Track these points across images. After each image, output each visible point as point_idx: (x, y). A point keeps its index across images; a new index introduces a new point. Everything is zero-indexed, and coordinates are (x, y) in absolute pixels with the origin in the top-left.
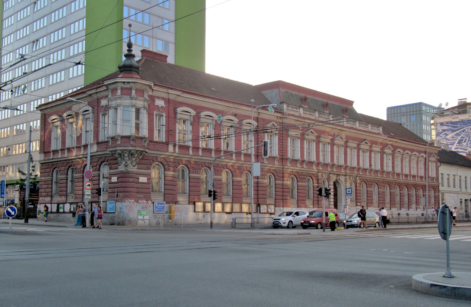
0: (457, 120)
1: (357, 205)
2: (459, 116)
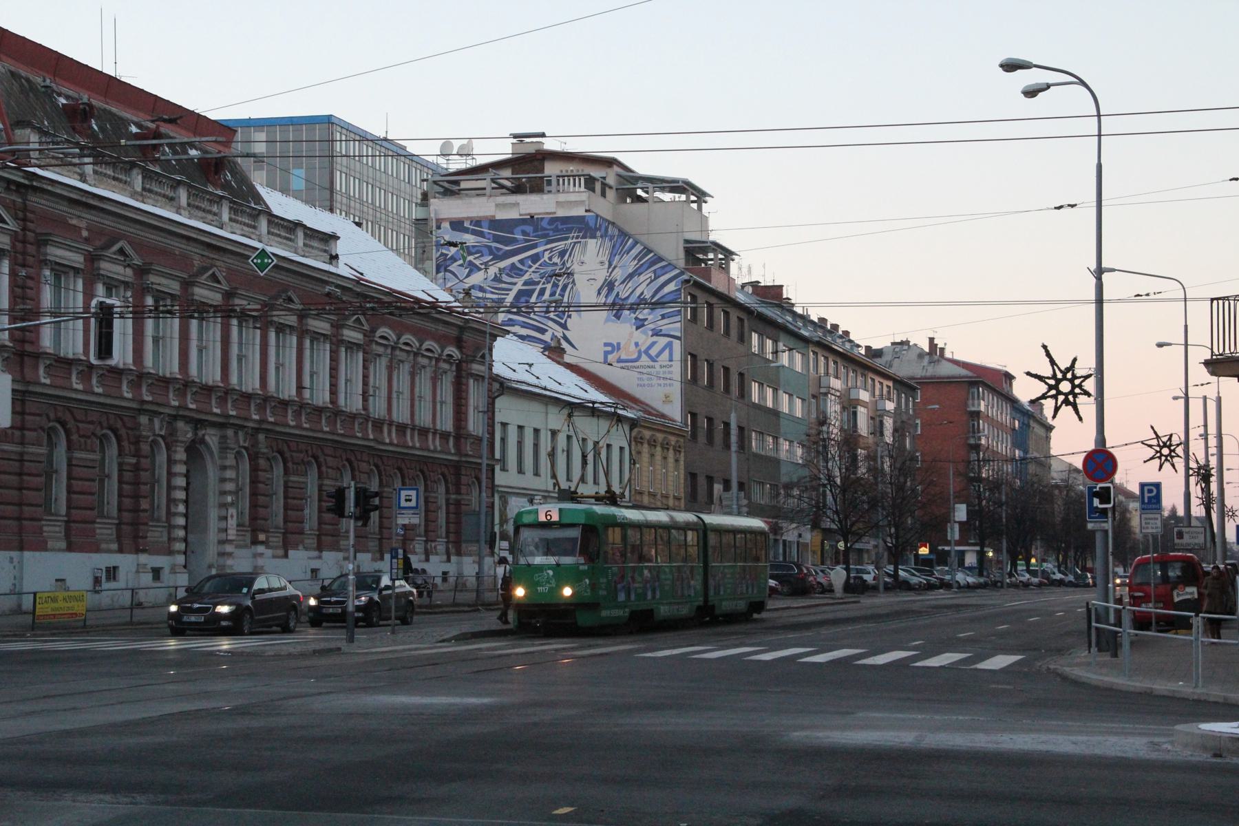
0: (513, 215)
1: (255, 542)
2: (519, 198)
